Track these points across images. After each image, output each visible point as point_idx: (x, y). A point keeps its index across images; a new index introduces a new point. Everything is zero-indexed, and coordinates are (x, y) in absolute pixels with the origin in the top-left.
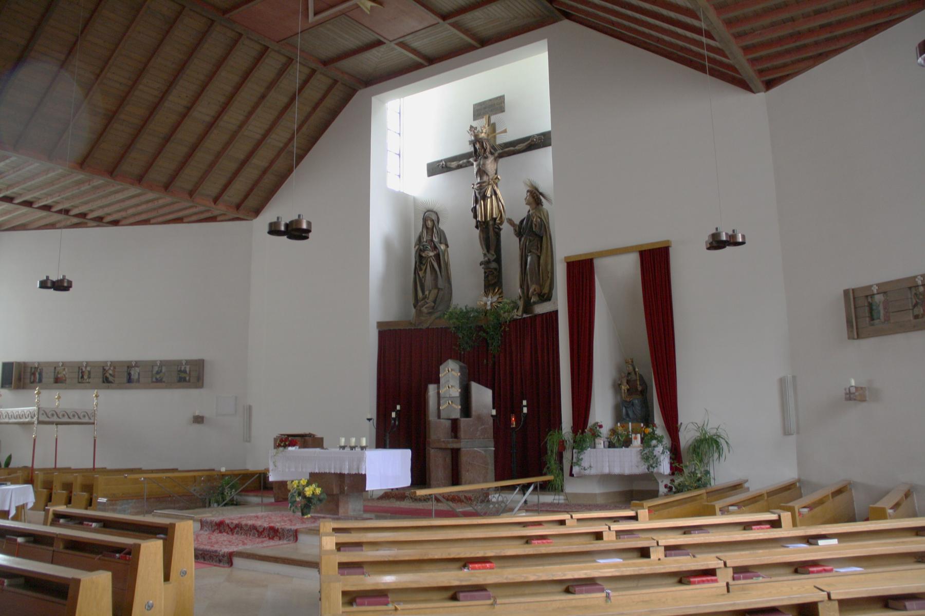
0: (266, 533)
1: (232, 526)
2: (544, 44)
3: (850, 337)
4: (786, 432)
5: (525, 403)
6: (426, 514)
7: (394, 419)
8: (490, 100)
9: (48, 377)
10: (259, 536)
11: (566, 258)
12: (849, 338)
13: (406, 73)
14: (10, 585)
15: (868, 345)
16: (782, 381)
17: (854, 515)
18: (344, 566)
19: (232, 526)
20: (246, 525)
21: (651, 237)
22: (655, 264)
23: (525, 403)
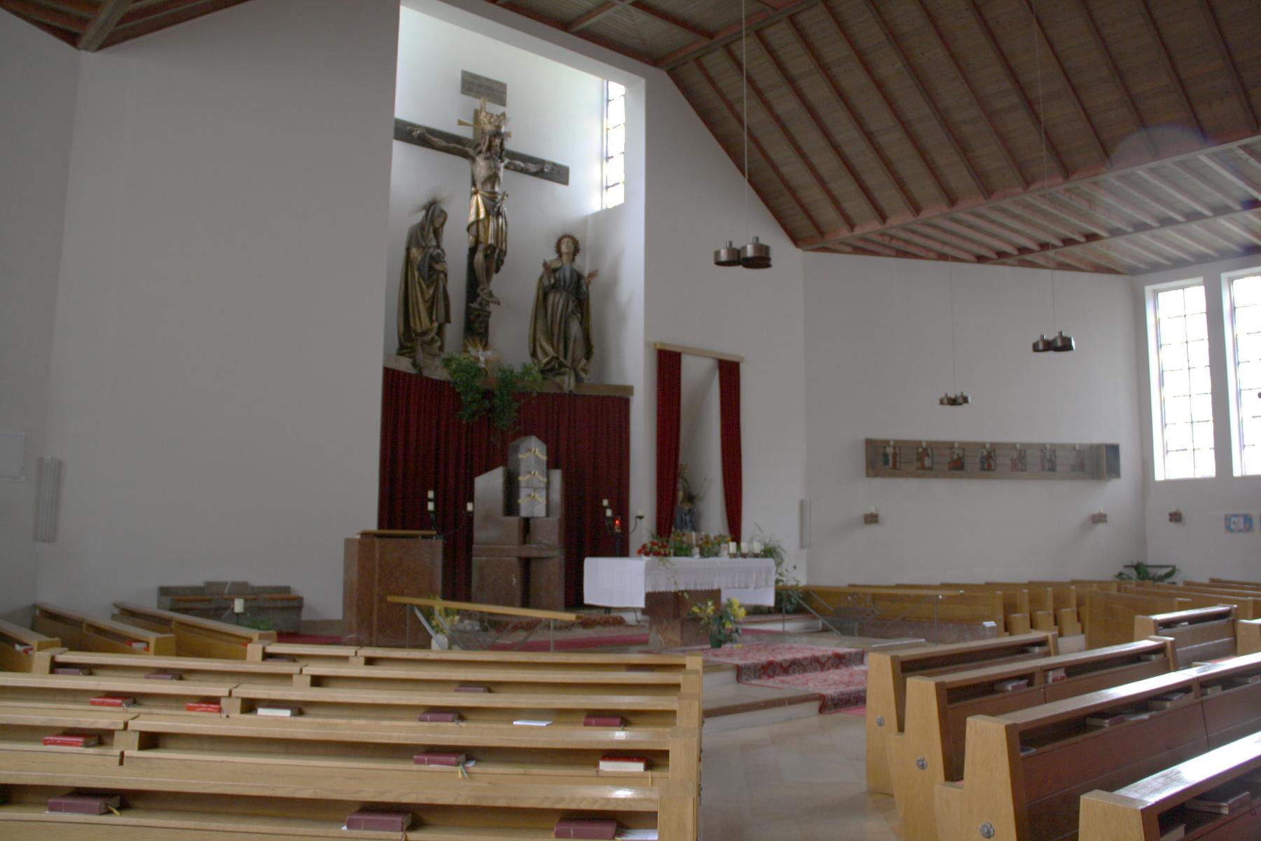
0: (829, 664)
1: (785, 665)
2: (1200, 279)
3: (868, 475)
4: (802, 547)
5: (431, 494)
6: (542, 647)
7: (613, 519)
8: (488, 80)
9: (972, 462)
10: (822, 670)
11: (662, 344)
12: (868, 475)
13: (528, 16)
14: (1111, 725)
15: (878, 483)
16: (802, 503)
17: (682, 625)
18: (666, 716)
19: (785, 665)
20: (805, 658)
21: (730, 351)
22: (729, 373)
23: (431, 494)
